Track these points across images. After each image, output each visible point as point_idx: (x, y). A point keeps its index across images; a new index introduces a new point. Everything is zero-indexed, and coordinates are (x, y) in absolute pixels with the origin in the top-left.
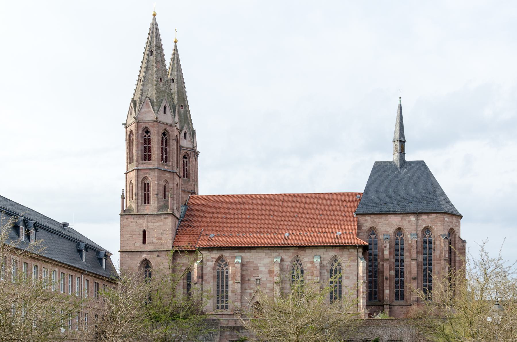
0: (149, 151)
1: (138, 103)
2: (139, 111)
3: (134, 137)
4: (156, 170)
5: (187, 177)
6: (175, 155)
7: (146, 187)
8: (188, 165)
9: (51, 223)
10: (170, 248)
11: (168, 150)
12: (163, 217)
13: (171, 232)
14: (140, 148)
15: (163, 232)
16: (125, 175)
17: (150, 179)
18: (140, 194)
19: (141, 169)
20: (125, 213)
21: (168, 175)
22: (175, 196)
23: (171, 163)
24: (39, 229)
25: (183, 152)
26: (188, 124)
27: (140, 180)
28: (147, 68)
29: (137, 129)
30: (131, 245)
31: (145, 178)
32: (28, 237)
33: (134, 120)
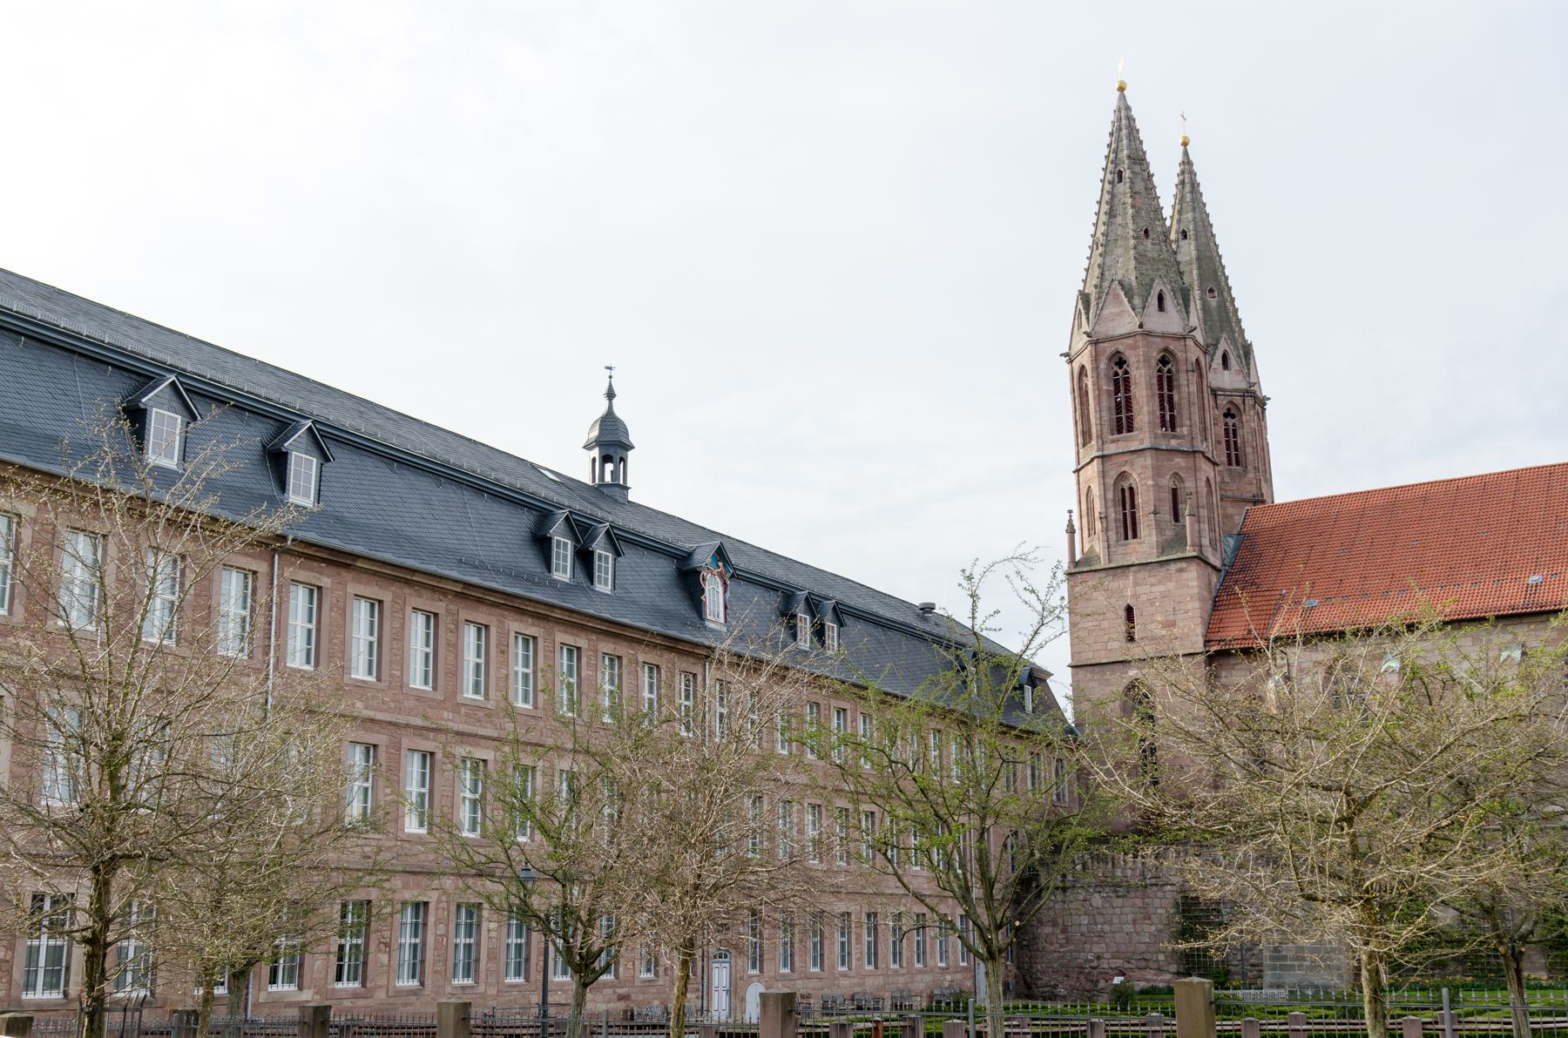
0: (1129, 408)
1: (1093, 298)
2: (1098, 316)
3: (1089, 382)
4: (1148, 453)
5: (1238, 464)
6: (1195, 409)
7: (1125, 498)
8: (1240, 432)
9: (887, 605)
10: (1200, 647)
11: (1176, 398)
12: (1173, 567)
13: (1197, 604)
14: (1105, 404)
15: (1177, 605)
16: (1074, 476)
17: (1135, 475)
18: (1112, 516)
19: (1110, 456)
20: (1079, 569)
21: (1180, 461)
22: (1204, 512)
23: (1185, 430)
24: (848, 620)
25: (1223, 401)
26: (1232, 331)
27: (1110, 481)
28: (1111, 214)
29: (1096, 359)
30: (1098, 646)
31: (1123, 476)
32: (819, 633)
33: (1086, 339)
